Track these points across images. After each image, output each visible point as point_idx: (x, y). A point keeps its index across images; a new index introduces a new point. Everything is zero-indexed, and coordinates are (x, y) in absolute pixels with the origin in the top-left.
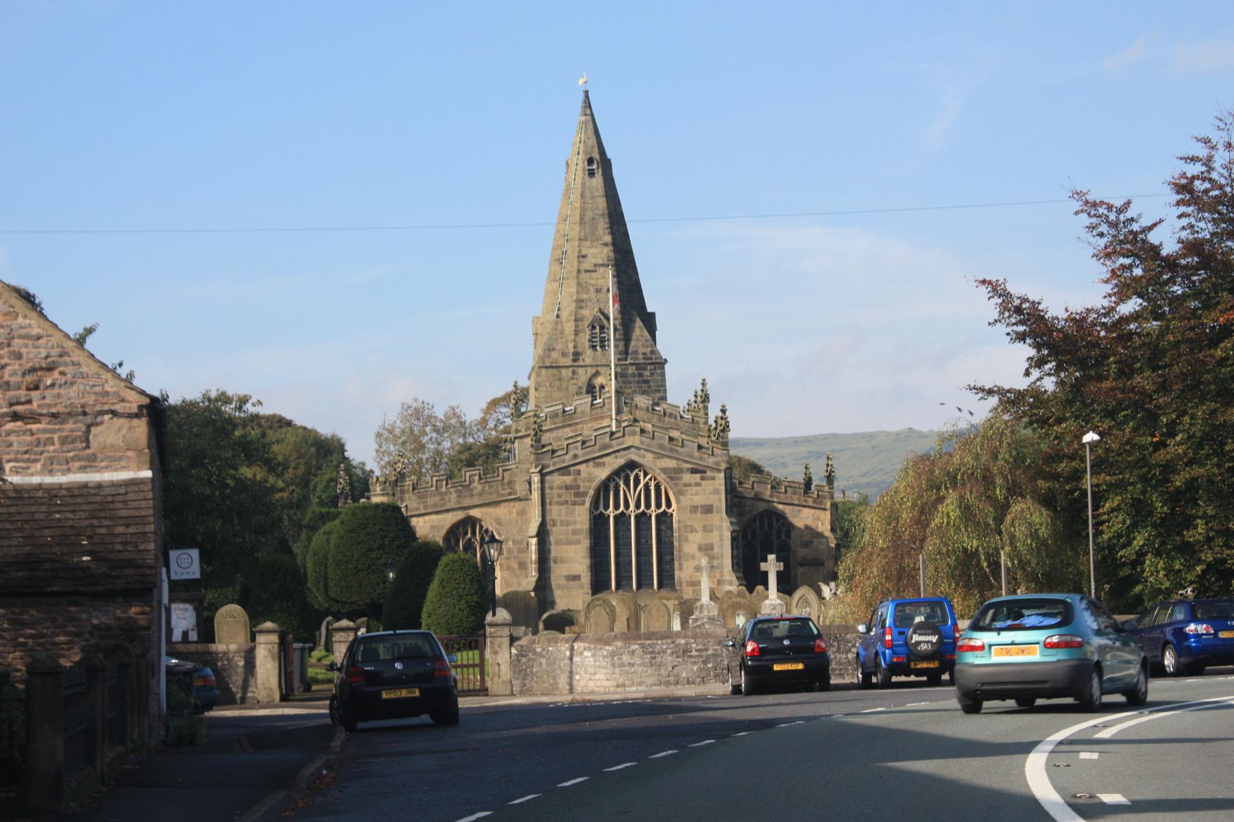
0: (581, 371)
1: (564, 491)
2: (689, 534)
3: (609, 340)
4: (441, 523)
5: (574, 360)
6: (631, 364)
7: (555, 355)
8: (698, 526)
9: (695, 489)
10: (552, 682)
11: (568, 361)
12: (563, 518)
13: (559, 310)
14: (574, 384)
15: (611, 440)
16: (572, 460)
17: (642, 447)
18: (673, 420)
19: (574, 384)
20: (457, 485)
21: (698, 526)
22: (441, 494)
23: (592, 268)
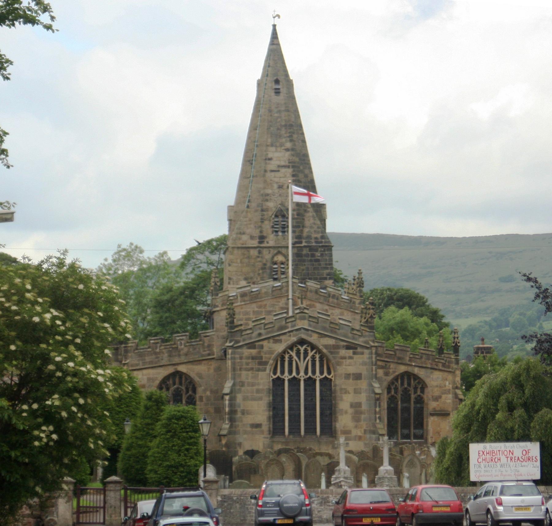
0: (265, 252)
1: (250, 361)
2: (343, 395)
3: (288, 227)
4: (155, 376)
5: (260, 242)
6: (305, 246)
7: (245, 238)
8: (351, 389)
9: (348, 361)
10: (242, 518)
11: (255, 243)
12: (250, 381)
13: (249, 201)
14: (260, 262)
15: (286, 323)
16: (256, 337)
17: (310, 328)
18: (335, 301)
19: (260, 262)
20: (168, 347)
21: (351, 389)
22: (156, 353)
23: (275, 168)
